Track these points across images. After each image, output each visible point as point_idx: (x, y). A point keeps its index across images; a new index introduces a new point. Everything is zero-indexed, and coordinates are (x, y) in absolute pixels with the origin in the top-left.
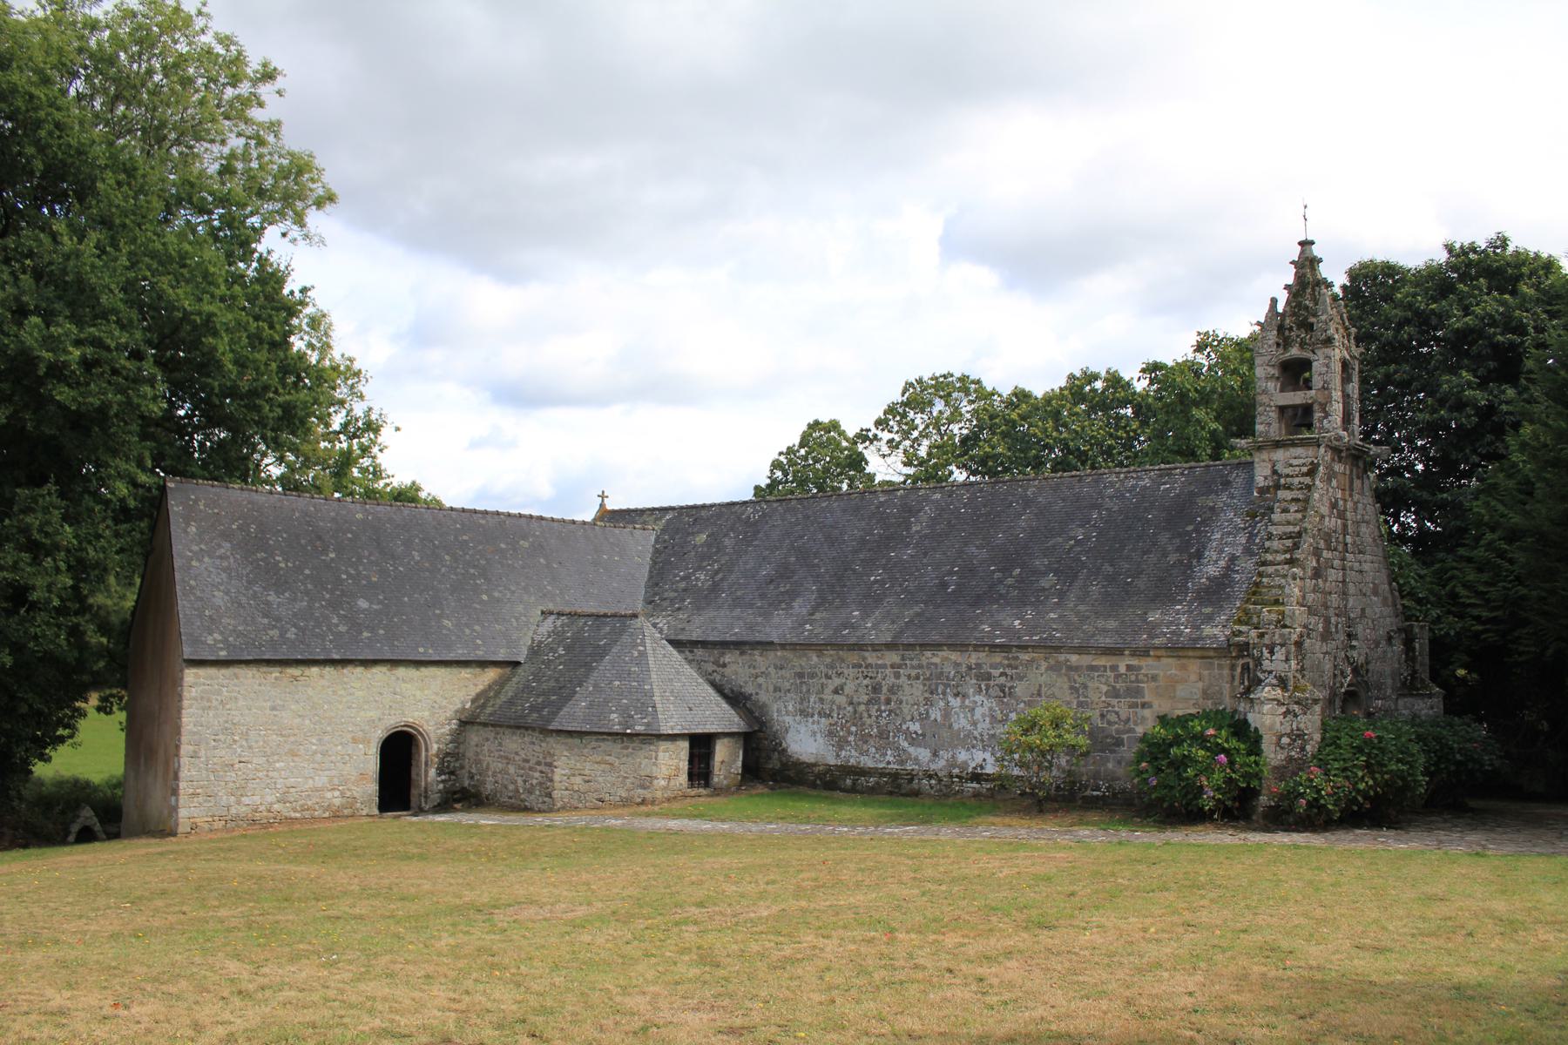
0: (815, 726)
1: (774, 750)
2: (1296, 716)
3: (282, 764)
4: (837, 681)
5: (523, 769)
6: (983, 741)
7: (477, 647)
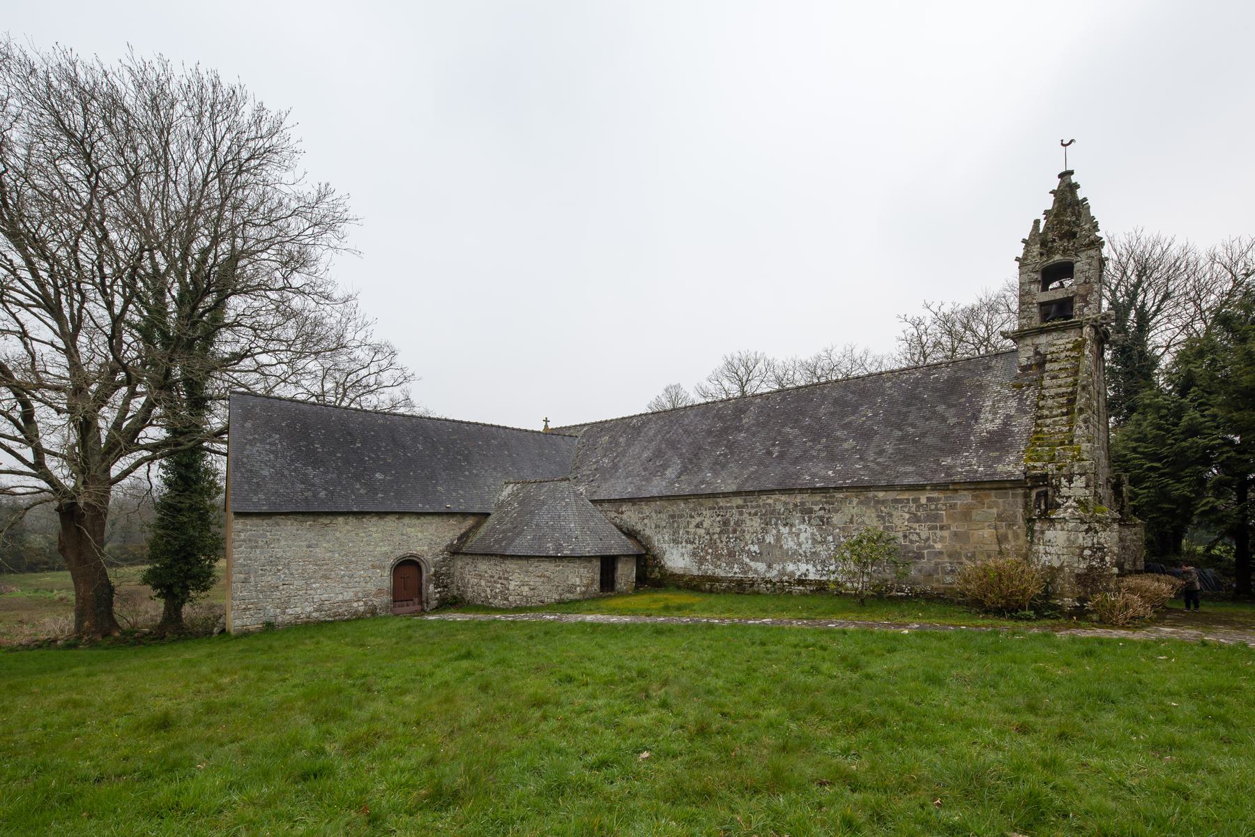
0: (684, 550)
1: (656, 566)
2: (1096, 532)
3: (318, 585)
4: (698, 519)
5: (490, 582)
6: (806, 556)
7: (461, 504)
